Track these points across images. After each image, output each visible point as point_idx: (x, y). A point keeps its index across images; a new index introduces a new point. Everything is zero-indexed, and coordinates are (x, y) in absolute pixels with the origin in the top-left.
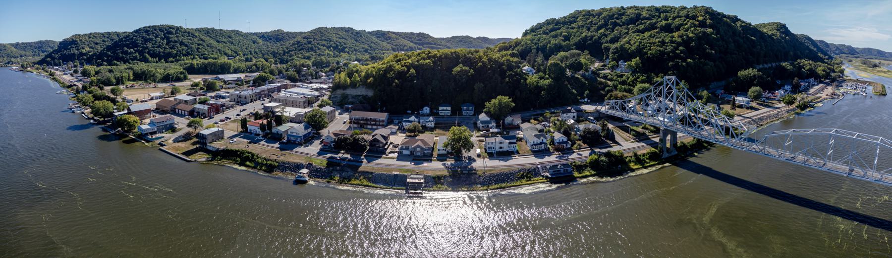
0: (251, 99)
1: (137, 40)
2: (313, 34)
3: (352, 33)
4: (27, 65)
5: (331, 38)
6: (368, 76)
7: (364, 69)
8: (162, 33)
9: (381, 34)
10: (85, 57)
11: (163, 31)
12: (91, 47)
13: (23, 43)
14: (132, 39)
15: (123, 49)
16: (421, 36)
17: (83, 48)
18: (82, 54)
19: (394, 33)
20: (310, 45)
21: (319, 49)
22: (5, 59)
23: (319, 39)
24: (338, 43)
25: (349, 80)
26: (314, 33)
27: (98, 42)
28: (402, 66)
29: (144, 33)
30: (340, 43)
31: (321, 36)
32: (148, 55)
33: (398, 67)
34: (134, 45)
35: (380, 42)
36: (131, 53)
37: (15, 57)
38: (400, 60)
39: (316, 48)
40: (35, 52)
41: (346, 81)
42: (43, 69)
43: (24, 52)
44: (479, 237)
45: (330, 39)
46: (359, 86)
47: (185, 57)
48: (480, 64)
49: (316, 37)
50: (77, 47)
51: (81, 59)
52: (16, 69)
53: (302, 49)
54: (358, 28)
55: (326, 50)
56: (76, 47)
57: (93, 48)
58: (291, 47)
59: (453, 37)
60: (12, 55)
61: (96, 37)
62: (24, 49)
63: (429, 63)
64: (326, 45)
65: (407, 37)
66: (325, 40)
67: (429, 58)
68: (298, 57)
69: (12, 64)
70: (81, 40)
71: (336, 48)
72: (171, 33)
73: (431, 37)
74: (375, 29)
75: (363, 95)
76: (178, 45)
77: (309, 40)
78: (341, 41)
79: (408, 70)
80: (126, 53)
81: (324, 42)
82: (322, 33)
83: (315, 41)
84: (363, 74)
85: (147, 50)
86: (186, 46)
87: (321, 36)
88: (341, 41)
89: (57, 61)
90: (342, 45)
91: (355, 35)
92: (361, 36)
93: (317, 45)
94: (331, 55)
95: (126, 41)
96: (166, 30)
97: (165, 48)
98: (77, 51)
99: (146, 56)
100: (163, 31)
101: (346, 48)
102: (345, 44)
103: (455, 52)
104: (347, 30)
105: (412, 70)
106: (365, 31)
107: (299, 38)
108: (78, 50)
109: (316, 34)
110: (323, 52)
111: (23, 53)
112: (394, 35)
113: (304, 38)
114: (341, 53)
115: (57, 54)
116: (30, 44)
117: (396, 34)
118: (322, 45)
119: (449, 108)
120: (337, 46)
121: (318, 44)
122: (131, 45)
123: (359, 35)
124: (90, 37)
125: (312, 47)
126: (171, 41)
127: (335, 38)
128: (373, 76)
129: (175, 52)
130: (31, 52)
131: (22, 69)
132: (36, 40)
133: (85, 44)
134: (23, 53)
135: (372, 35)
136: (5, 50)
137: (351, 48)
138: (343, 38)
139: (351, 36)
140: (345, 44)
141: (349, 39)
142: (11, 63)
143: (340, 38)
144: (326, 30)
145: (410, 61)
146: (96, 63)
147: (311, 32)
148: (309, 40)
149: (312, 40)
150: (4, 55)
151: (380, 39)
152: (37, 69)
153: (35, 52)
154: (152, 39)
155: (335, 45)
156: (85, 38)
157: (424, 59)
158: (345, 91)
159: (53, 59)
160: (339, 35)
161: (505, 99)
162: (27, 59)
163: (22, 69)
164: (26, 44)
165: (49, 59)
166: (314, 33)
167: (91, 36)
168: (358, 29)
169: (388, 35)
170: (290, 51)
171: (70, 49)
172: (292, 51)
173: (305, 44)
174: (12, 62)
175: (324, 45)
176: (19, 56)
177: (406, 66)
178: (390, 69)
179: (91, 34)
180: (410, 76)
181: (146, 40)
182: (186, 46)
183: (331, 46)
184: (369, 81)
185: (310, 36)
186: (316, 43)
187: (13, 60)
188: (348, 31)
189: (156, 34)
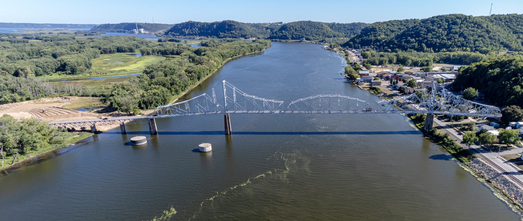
1: (421, 31)
4: (334, 46)
8: (447, 23)
10: (378, 44)
11: (448, 22)
12: (387, 35)
13: (338, 24)
14: (418, 28)
15: (406, 38)
17: (379, 35)
18: (377, 41)
22: (321, 37)
27: (394, 30)
29: (430, 24)
32: (425, 45)
34: (417, 34)
36: (412, 42)
37: (329, 37)
40: (347, 34)
42: (344, 51)
43: (337, 33)
44: (138, 89)
47: (517, 34)
50: (375, 34)
51: (375, 45)
52: (326, 48)
56: (374, 34)
57: (388, 36)
60: (327, 34)
61: (393, 25)
62: (338, 30)
69: (325, 43)
70: (380, 28)
72: (455, 23)
76: (457, 36)
80: (408, 42)
85: (426, 40)
86: (465, 37)
89: (357, 45)
95: (412, 31)
96: (452, 21)
97: (443, 39)
98: (374, 38)
99: (423, 45)
100: (448, 22)
108: (375, 36)
111: (337, 33)
115: (359, 39)
116: (344, 25)
122: (414, 35)
124: (388, 25)
126: (451, 33)
129: (450, 43)
130: (344, 34)
131: (330, 49)
132: (350, 22)
133: (382, 32)
134: (337, 33)
136: (322, 29)
142: (324, 42)
146: (383, 49)
150: (320, 33)
152: (340, 50)
153: (347, 34)
154: (435, 29)
156: (384, 26)
159: (355, 42)
162: (338, 40)
163: (330, 49)
164: (341, 25)
165: (351, 43)
167: (390, 24)
171: (369, 36)
174: (325, 41)
176: (333, 36)
179: (390, 22)
181: (429, 31)
182: (465, 37)
187: (327, 39)
189: (440, 24)
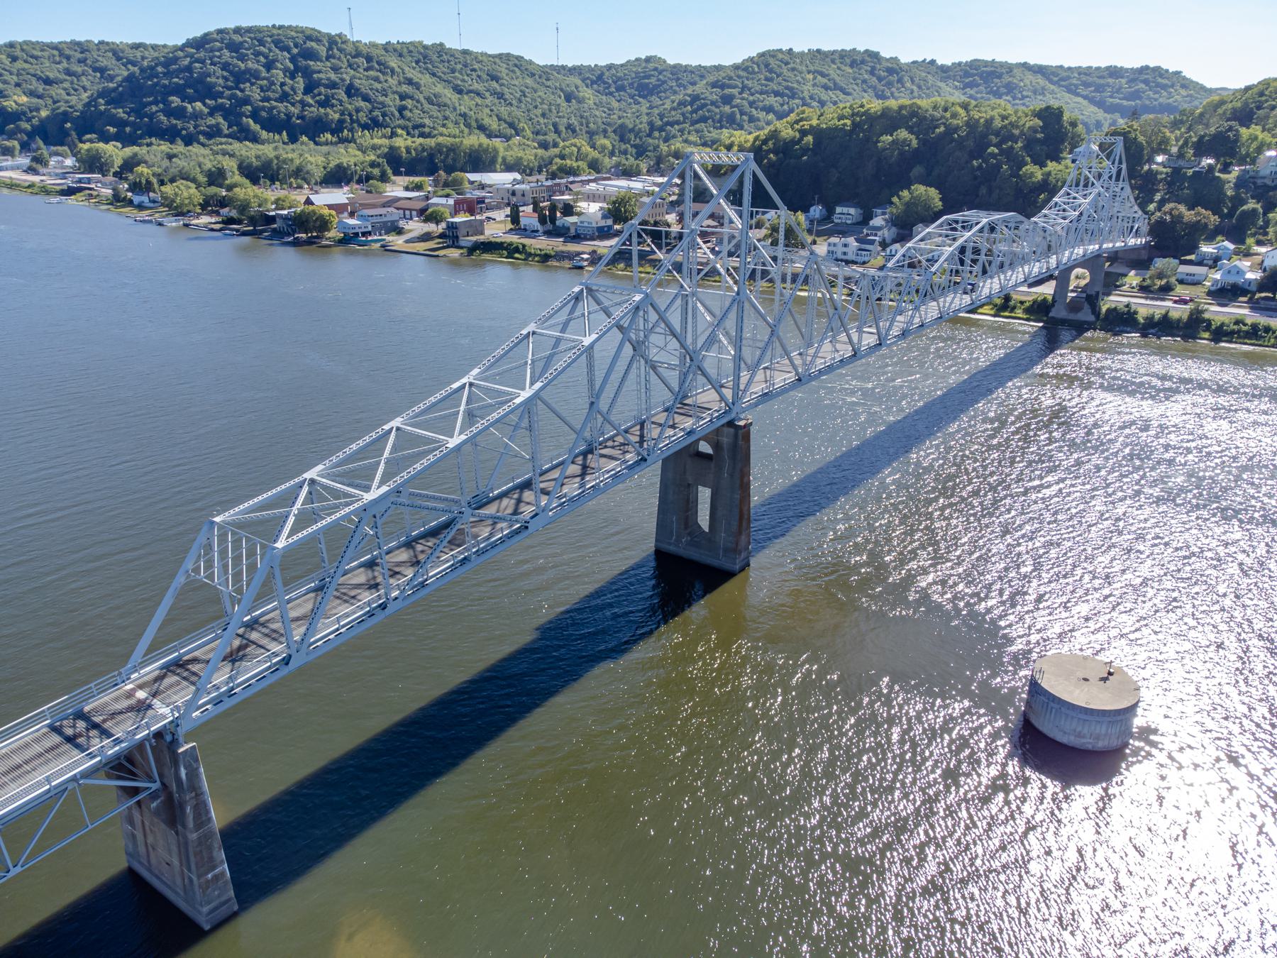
5: (795, 85)
16: (1146, 82)
19: (1040, 70)
23: (758, 88)
53: (704, 120)
58: (673, 113)
65: (1086, 85)
66: (777, 94)
73: (1186, 84)
74: (966, 57)
79: (801, 139)
81: (772, 100)
82: (771, 71)
92: (900, 81)
109: (753, 72)
112: (1029, 77)
118: (763, 109)
119: (852, 211)
121: (751, 104)
123: (895, 77)
139: (864, 81)
149: (735, 91)
161: (933, 193)
166: (746, 69)
169: (1006, 79)
173: (713, 103)
175: (769, 110)
186: (745, 103)
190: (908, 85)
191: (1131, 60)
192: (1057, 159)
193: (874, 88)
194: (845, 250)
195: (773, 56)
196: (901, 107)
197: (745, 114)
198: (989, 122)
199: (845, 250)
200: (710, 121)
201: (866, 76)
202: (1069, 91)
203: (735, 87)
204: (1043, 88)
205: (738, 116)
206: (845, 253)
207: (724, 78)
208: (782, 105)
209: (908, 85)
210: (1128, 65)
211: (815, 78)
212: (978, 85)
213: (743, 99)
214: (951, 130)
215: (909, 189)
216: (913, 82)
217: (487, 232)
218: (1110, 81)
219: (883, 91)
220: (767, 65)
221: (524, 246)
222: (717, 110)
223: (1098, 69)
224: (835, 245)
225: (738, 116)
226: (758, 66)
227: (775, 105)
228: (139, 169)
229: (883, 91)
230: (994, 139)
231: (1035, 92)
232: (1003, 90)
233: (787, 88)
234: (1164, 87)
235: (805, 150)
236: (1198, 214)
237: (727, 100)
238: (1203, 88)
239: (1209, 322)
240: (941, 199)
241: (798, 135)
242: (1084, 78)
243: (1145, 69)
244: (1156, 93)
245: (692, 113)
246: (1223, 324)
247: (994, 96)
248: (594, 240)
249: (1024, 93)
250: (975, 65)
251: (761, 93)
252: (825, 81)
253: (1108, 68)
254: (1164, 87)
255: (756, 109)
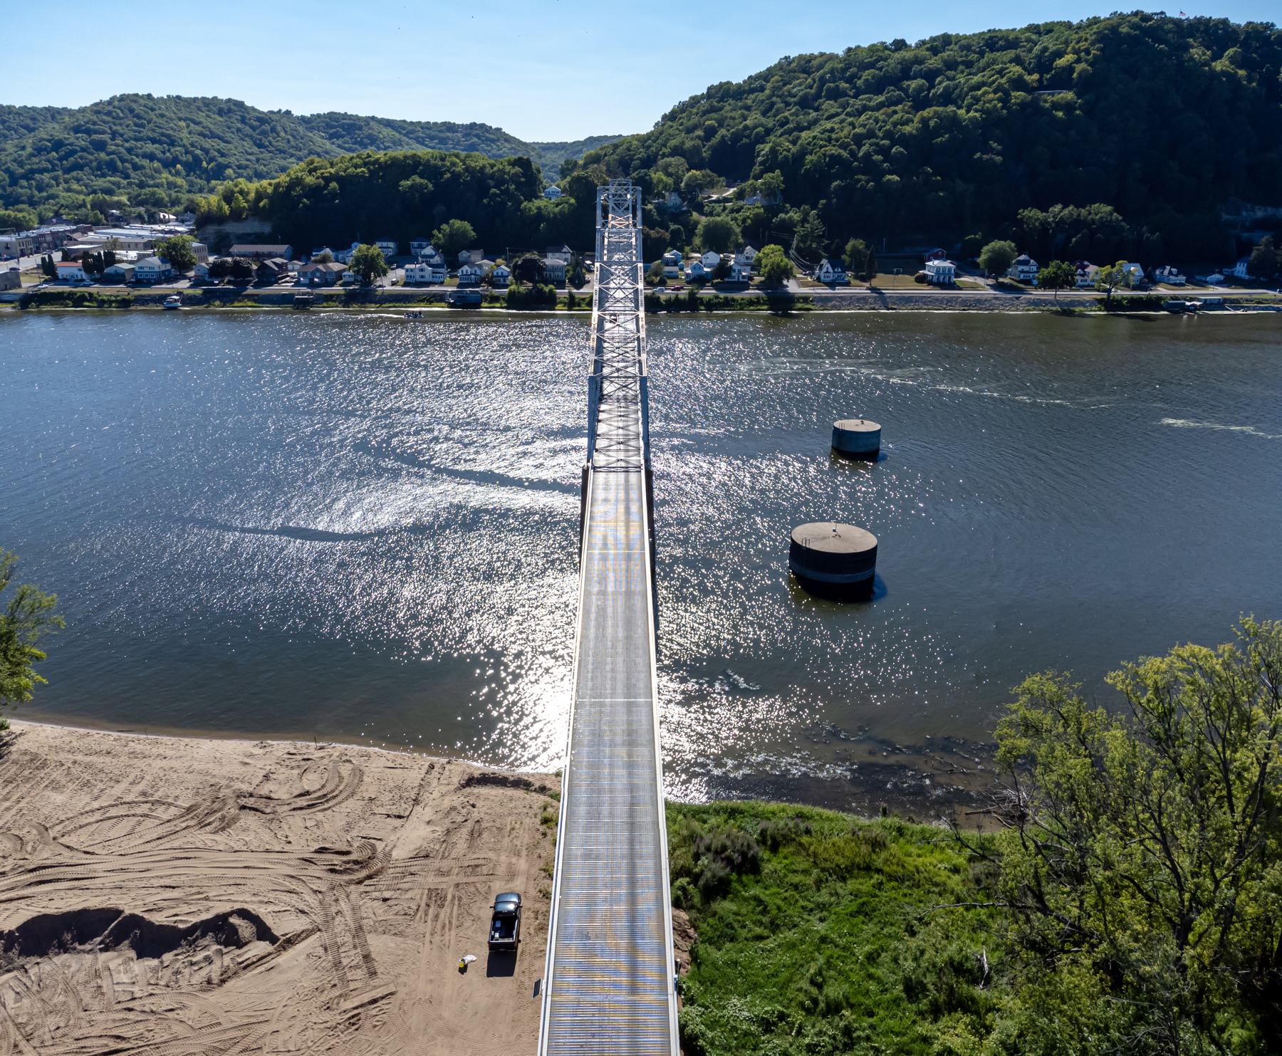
0: (22, 250)
2: (105, 118)
3: (243, 120)
5: (171, 132)
6: (260, 195)
7: (252, 187)
9: (342, 126)
16: (477, 136)
19: (389, 123)
20: (103, 155)
21: (136, 167)
23: (131, 134)
24: (198, 152)
25: (227, 207)
26: (109, 114)
28: (317, 178)
30: (206, 151)
31: (136, 125)
33: (310, 180)
35: (338, 150)
38: (315, 169)
39: (127, 165)
41: (220, 208)
45: (168, 136)
46: (247, 216)
48: (448, 175)
49: (118, 128)
53: (79, 167)
54: (263, 102)
55: (160, 173)
58: (35, 160)
59: (591, 138)
63: (362, 172)
64: (160, 155)
65: (432, 138)
66: (154, 141)
67: (365, 164)
68: (69, 190)
71: (193, 167)
73: (508, 139)
74: (324, 110)
75: (255, 234)
77: (95, 137)
78: (208, 143)
79: (327, 185)
81: (150, 147)
82: (139, 117)
83: (119, 141)
84: (252, 196)
87: (136, 125)
88: (208, 143)
90: (212, 160)
91: (254, 128)
92: (273, 130)
93: (128, 157)
94: (181, 187)
101: (227, 166)
102: (223, 155)
103: (414, 156)
104: (225, 106)
105: (334, 185)
106: (288, 112)
107: (55, 130)
109: (118, 118)
110: (153, 178)
112: (387, 132)
113: (77, 130)
114: (213, 182)
117: (393, 128)
118: (145, 156)
119: (391, 245)
120: (197, 160)
121: (129, 150)
123: (267, 127)
125: (112, 160)
127: (184, 134)
128: (267, 196)
135: (311, 129)
137: (246, 167)
138: (213, 135)
139: (239, 130)
140: (223, 155)
141: (235, 139)
143: (205, 136)
144: (150, 104)
145: (332, 171)
147: (98, 108)
148: (95, 137)
149: (106, 137)
151: (340, 142)
155: (190, 158)
157: (356, 166)
158: (222, 228)
160: (198, 123)
161: (467, 226)
166: (109, 114)
168: (264, 107)
169: (366, 131)
170: (33, 171)
172: (42, 171)
173: (83, 150)
175: (151, 157)
177: (324, 178)
178: (297, 182)
180: (329, 193)
183: (176, 161)
184: (261, 204)
185: (95, 123)
186: (122, 150)
188: (230, 110)
190: (282, 134)
191: (462, 118)
192: (537, 197)
193: (251, 137)
194: (422, 273)
195: (135, 101)
196: (406, 157)
197: (126, 161)
198: (483, 168)
199: (422, 273)
200: (86, 168)
201: (239, 125)
202: (418, 142)
203: (104, 132)
204: (399, 140)
205: (119, 163)
206: (422, 277)
207: (87, 123)
208: (164, 153)
209: (282, 134)
210: (459, 122)
211: (188, 126)
212: (343, 136)
213: (117, 145)
214: (456, 176)
215: (448, 223)
216: (286, 132)
217: (24, 285)
218: (449, 134)
219: (260, 140)
220: (132, 111)
221: (90, 294)
222: (91, 157)
223: (435, 124)
224: (412, 270)
225: (119, 163)
226: (122, 111)
227: (157, 152)
228: (809, 158)
229: (260, 140)
230: (491, 183)
231: (394, 143)
232: (366, 141)
233: (163, 134)
234: (493, 141)
235: (333, 195)
236: (658, 232)
237: (100, 146)
238: (520, 142)
239: (701, 299)
240: (473, 230)
241: (323, 182)
242: (428, 132)
243: (473, 125)
244: (488, 145)
245: (61, 159)
246: (710, 300)
247: (360, 145)
248: (161, 284)
249: (386, 144)
250: (332, 116)
251: (137, 140)
252: (199, 128)
253: (444, 124)
254: (493, 141)
255: (137, 156)
